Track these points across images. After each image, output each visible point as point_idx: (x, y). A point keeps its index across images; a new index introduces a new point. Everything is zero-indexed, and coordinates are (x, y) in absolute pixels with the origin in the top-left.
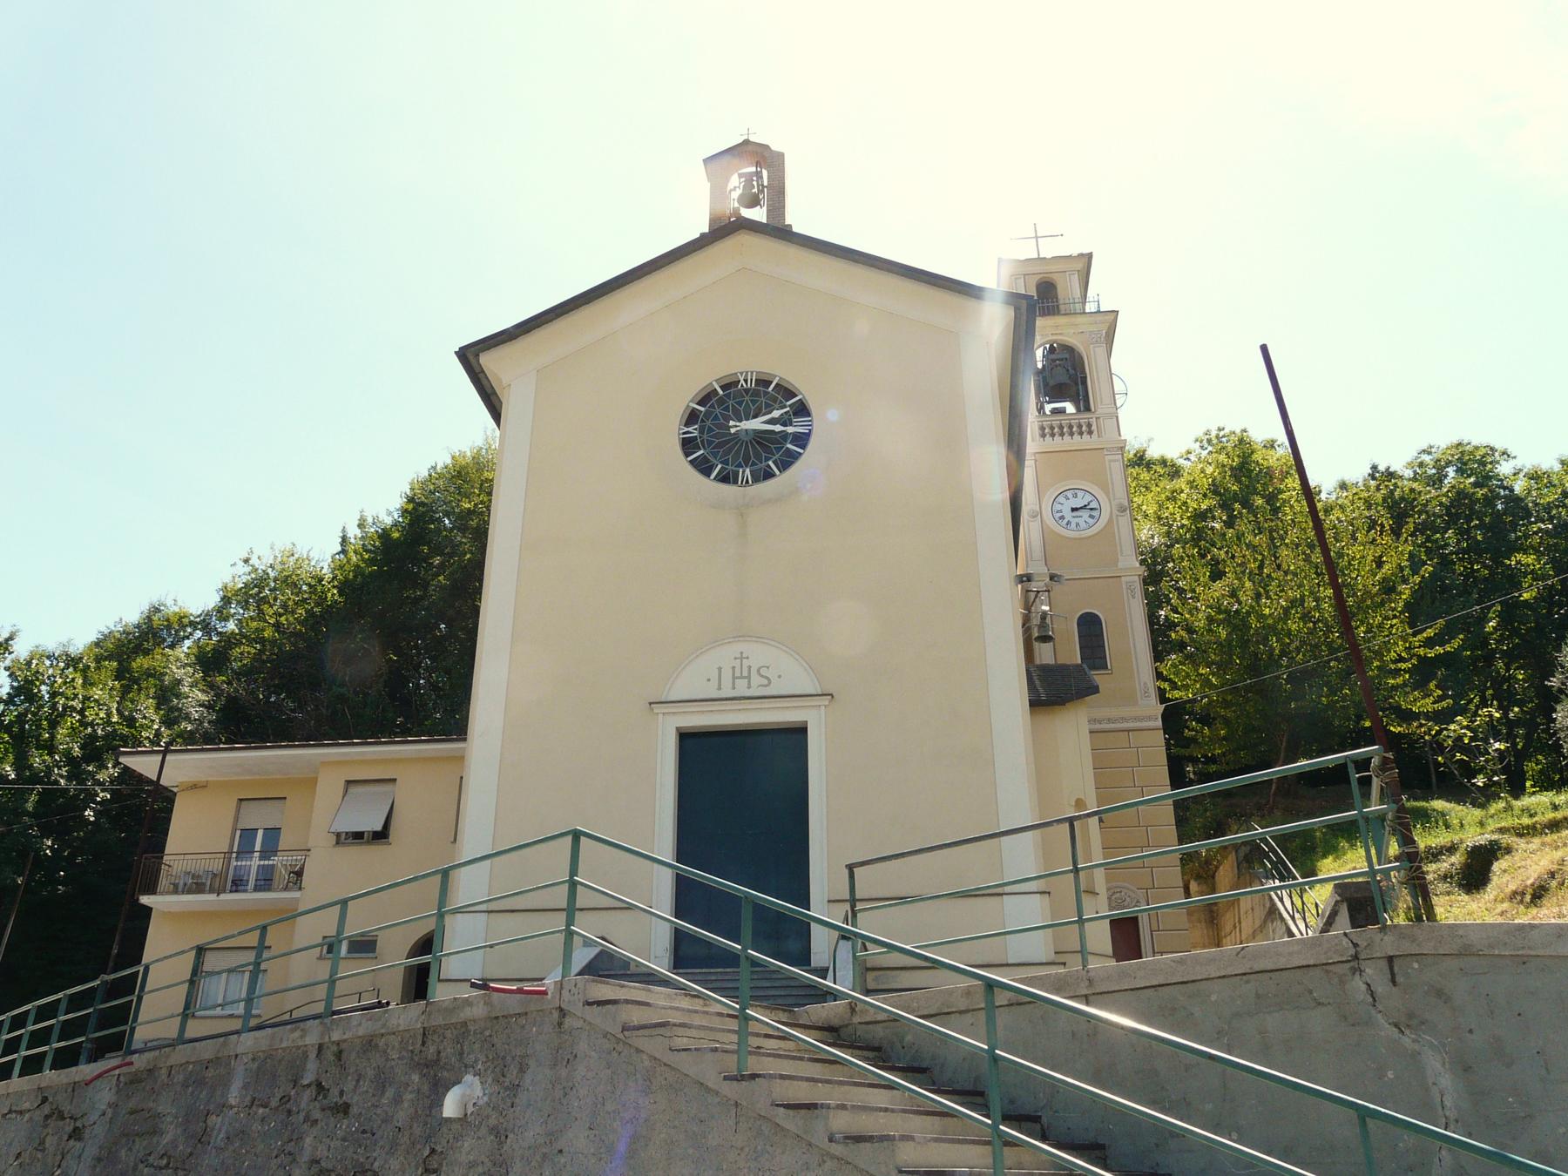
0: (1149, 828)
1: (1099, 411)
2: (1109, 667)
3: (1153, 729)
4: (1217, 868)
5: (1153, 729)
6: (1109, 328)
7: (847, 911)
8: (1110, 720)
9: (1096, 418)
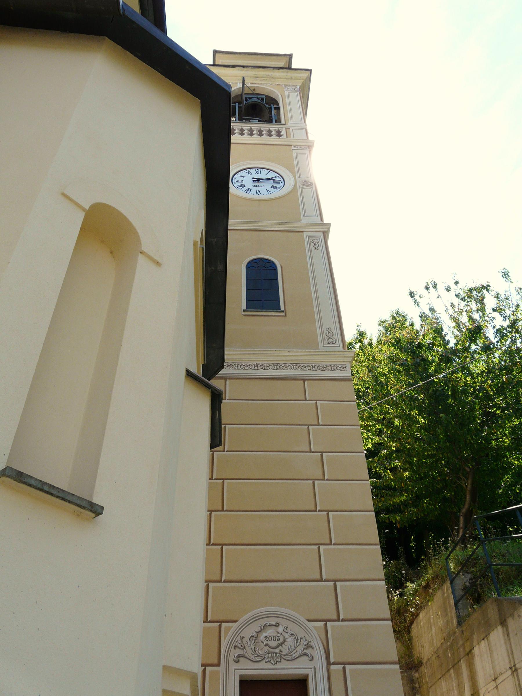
0: (331, 514)
1: (289, 125)
2: (282, 308)
3: (274, 199)
4: (416, 615)
5: (274, 199)
6: (303, 83)
7: (202, 230)
8: (277, 366)
9: (286, 129)
